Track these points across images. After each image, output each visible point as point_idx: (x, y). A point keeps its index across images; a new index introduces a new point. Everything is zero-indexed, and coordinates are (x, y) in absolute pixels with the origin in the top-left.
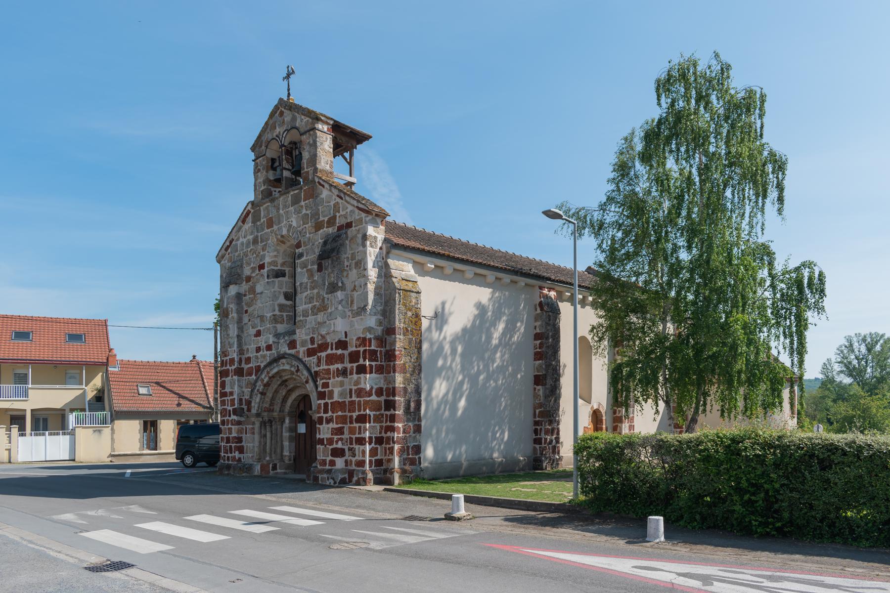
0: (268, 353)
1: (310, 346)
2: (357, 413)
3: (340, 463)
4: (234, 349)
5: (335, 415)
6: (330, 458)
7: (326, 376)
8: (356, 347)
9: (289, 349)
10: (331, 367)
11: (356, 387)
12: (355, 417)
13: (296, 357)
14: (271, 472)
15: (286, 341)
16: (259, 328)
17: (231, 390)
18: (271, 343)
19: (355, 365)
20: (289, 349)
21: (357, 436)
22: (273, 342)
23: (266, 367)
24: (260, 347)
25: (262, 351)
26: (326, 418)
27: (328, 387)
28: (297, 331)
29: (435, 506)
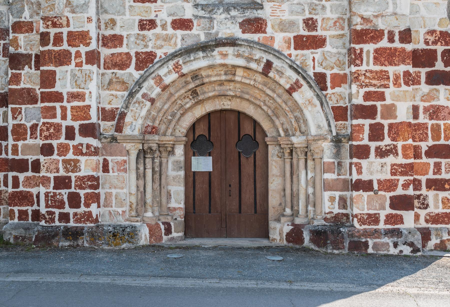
2: (431, 142)
8: (427, 43)
9: (243, 32)
10: (391, 70)
11: (427, 104)
14: (165, 238)
15: (234, 17)
20: (243, 32)
21: (431, 176)
28: (268, 6)
29: (370, 285)
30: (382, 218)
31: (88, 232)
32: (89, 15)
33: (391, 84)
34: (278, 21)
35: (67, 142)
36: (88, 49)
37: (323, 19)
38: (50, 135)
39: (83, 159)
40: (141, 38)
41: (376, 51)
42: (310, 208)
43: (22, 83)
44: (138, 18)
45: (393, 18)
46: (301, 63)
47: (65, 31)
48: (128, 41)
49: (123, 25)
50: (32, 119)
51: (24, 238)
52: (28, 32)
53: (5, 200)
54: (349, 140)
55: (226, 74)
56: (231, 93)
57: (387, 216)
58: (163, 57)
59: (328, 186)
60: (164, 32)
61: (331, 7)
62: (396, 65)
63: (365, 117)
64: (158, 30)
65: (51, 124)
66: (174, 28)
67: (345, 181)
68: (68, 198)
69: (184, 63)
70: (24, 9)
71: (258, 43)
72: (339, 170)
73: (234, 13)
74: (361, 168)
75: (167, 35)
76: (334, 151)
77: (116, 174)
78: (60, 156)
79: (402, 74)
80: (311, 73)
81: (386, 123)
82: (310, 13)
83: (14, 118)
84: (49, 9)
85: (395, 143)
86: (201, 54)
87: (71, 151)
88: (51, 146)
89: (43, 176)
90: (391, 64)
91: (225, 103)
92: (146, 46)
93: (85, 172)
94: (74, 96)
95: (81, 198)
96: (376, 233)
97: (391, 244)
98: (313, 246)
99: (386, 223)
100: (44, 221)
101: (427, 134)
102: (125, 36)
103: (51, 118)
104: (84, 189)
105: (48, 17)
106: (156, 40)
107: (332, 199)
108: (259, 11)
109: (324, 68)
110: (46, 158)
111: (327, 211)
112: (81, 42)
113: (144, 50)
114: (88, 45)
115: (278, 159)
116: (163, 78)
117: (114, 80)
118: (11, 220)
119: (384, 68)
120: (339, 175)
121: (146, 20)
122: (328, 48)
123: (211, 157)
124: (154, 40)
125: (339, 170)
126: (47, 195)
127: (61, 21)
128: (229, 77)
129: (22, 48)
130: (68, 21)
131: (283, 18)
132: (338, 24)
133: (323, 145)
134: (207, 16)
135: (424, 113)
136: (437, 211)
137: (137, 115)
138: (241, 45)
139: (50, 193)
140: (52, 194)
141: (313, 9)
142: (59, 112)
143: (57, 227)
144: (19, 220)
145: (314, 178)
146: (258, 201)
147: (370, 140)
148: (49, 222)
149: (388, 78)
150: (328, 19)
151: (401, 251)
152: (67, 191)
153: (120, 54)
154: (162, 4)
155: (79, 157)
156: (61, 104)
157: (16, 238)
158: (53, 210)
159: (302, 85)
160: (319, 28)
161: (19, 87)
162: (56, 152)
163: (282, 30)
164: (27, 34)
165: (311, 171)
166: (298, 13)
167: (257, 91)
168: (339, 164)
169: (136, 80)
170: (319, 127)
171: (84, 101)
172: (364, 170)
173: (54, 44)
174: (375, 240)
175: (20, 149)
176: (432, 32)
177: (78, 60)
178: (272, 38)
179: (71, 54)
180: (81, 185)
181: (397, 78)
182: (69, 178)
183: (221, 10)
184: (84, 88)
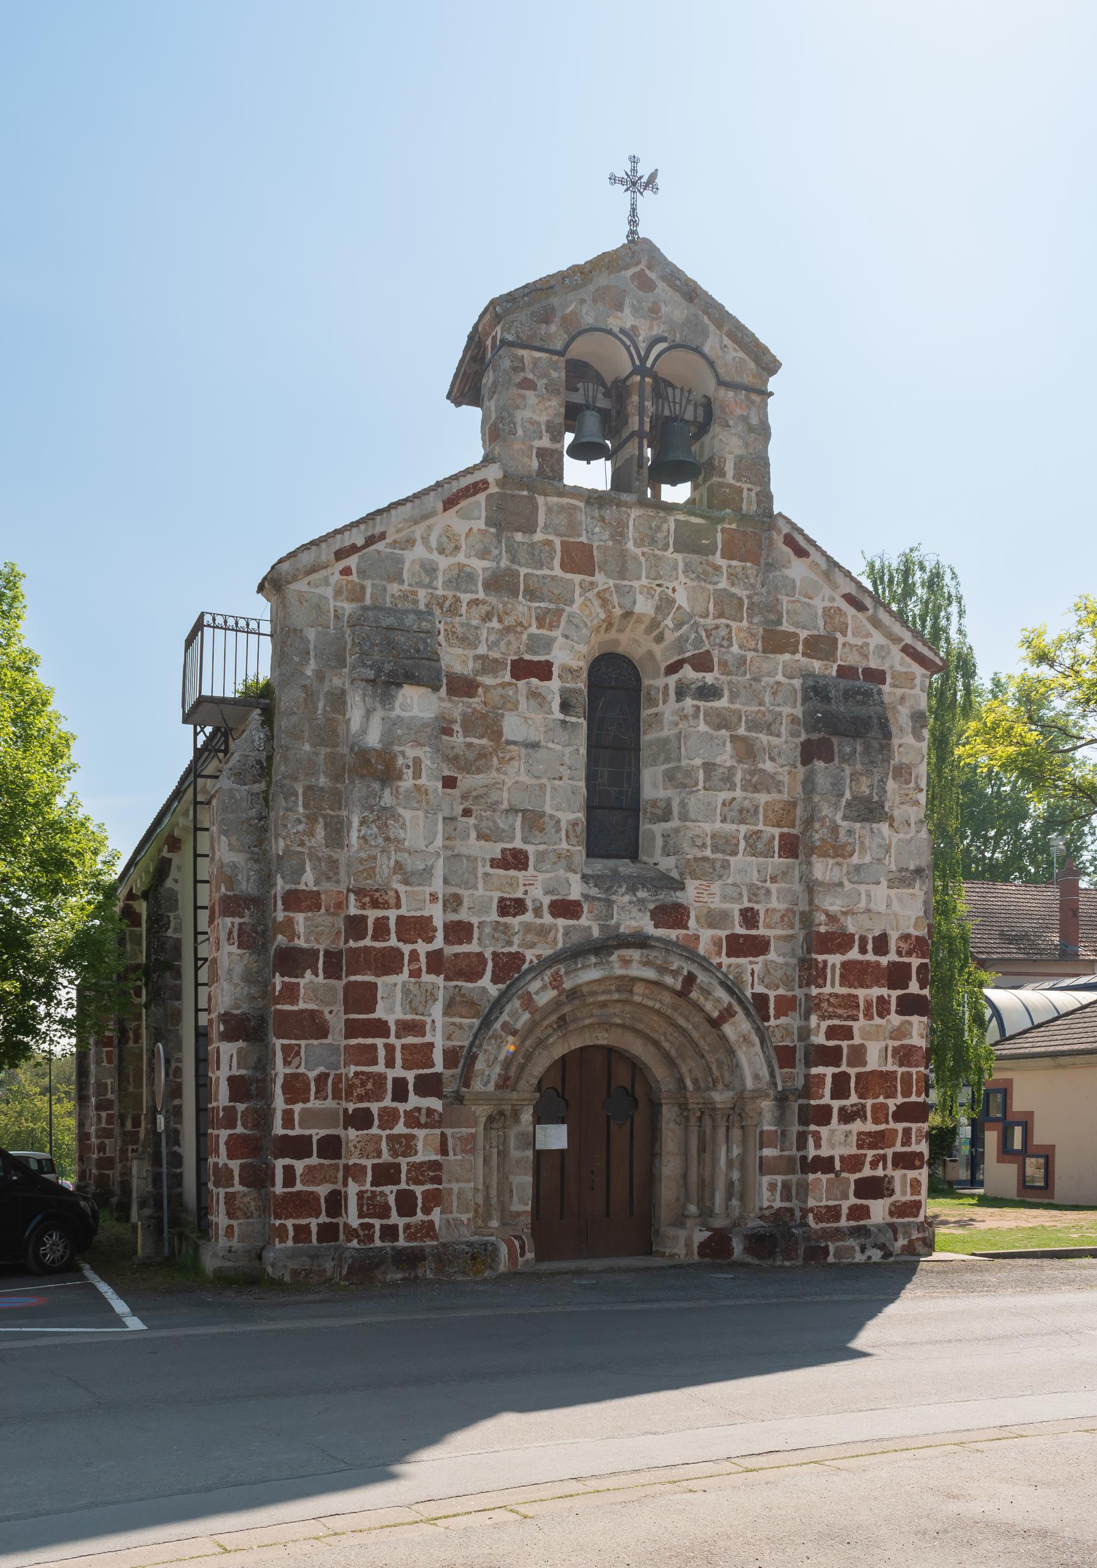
2: (900, 1100)
3: (879, 1210)
5: (869, 1103)
8: (899, 953)
9: (656, 926)
10: (862, 993)
11: (897, 1043)
12: (892, 1108)
13: (688, 951)
15: (642, 901)
16: (518, 844)
19: (895, 993)
20: (656, 926)
21: (899, 1148)
26: (842, 1110)
28: (692, 885)
30: (845, 1211)
31: (433, 1255)
32: (432, 890)
33: (861, 1015)
34: (705, 911)
35: (395, 1104)
36: (431, 947)
37: (767, 910)
38: (367, 1094)
39: (420, 1133)
40: (501, 928)
41: (844, 965)
42: (735, 1202)
43: (301, 1002)
44: (496, 895)
45: (865, 916)
46: (735, 978)
47: (392, 914)
48: (480, 933)
49: (472, 905)
50: (318, 1065)
51: (308, 1273)
52: (311, 910)
53: (241, 1210)
54: (800, 1097)
55: (618, 990)
56: (618, 1021)
57: (850, 1208)
58: (536, 961)
59: (764, 1167)
60: (538, 921)
61: (778, 892)
62: (868, 987)
63: (827, 1065)
64: (528, 917)
65: (369, 1075)
66: (554, 915)
67: (791, 1159)
68: (396, 1200)
69: (566, 973)
70: (303, 871)
71: (675, 944)
72: (783, 1142)
73: (642, 894)
74: (820, 1138)
75: (542, 925)
76: (777, 1114)
77: (459, 1157)
78: (384, 1129)
79: (875, 1000)
80: (748, 993)
81: (853, 1072)
82: (750, 900)
83: (287, 1063)
84: (365, 875)
85: (863, 1101)
86: (593, 959)
87: (402, 1120)
88: (368, 1111)
89: (355, 1164)
90: (862, 987)
91: (600, 1036)
92: (509, 943)
93: (424, 1154)
94: (407, 1028)
95: (417, 1198)
96: (838, 1234)
97: (858, 1248)
98: (749, 1259)
99: (849, 1218)
100: (355, 1241)
101: (895, 1087)
102: (476, 925)
103: (369, 1065)
104: (422, 1184)
105: (365, 889)
106: (525, 934)
107: (772, 1187)
108: (679, 894)
109: (766, 987)
110: (360, 1132)
111: (766, 1204)
112: (420, 936)
113: (506, 950)
114: (430, 940)
115: (677, 1126)
116: (534, 997)
117: (458, 999)
118: (280, 1242)
119: (853, 991)
120: (782, 1150)
121: (510, 899)
122: (772, 956)
123: (564, 1127)
124: (521, 933)
125: (783, 1142)
126: (360, 1195)
127: (386, 898)
128: (624, 996)
129: (302, 937)
130: (398, 897)
131: (712, 906)
132: (786, 919)
133: (762, 1105)
134: (603, 896)
135: (893, 1056)
136: (904, 1199)
137: (492, 1058)
138: (652, 947)
139: (366, 1192)
140: (369, 1194)
141: (754, 894)
142: (381, 1053)
143: (381, 1249)
144: (295, 1243)
145: (743, 1159)
147: (832, 1098)
148: (363, 1241)
149: (858, 1006)
150: (774, 910)
151: (869, 1258)
152: (395, 1188)
153: (468, 954)
154: (536, 873)
155: (415, 1131)
156: (385, 1040)
157: (295, 1273)
158: (371, 1221)
159: (736, 1012)
160: (761, 924)
161: (295, 1008)
162: (376, 1122)
163: (711, 926)
164: (310, 914)
165: (738, 1146)
166: (733, 900)
167: (655, 1018)
168: (783, 1133)
169: (492, 1000)
170: (756, 1077)
171: (423, 1035)
172: (824, 1142)
173: (375, 938)
174: (837, 1244)
175: (296, 1117)
176: (905, 937)
177: (414, 967)
178: (697, 938)
179: (402, 954)
180: (417, 1177)
181: (868, 1004)
182: (398, 1166)
183: (623, 890)
184: (423, 1014)
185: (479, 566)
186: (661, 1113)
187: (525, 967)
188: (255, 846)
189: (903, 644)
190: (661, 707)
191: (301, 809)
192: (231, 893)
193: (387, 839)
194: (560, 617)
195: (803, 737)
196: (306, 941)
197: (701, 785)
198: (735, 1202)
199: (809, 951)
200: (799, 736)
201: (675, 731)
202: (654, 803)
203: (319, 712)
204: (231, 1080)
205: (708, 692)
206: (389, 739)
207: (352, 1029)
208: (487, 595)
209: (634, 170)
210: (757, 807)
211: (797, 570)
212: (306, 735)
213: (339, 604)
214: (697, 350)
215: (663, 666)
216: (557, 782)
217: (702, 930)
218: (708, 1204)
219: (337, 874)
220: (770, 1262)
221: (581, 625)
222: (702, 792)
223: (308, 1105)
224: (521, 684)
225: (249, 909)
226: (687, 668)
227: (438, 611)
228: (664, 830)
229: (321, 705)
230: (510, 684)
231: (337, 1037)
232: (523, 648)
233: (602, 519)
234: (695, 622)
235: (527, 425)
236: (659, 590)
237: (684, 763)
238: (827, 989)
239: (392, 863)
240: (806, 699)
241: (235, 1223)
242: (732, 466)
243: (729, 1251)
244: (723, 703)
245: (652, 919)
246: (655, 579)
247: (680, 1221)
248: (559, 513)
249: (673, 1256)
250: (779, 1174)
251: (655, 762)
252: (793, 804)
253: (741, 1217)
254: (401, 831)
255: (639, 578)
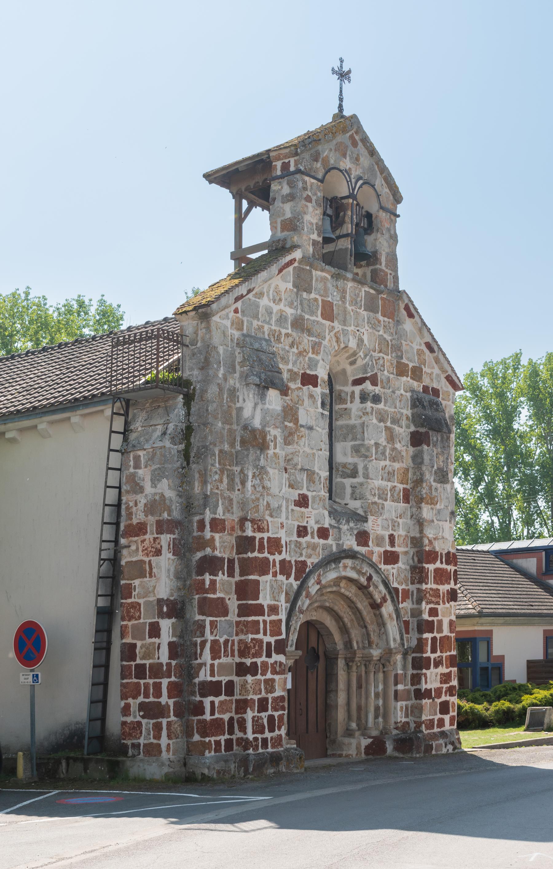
0: (322, 541)
1: (389, 548)
4: (280, 520)
5: (444, 655)
6: (439, 716)
7: (433, 599)
9: (358, 545)
13: (367, 559)
15: (351, 529)
16: (304, 491)
17: (273, 603)
18: (326, 526)
20: (358, 545)
22: (330, 525)
23: (317, 567)
24: (305, 528)
25: (309, 536)
27: (437, 615)
28: (371, 518)
34: (376, 535)
42: (380, 720)
44: (296, 523)
52: (221, 532)
53: (174, 733)
54: (413, 652)
72: (405, 681)
75: (314, 543)
76: (403, 663)
85: (442, 654)
90: (441, 584)
97: (444, 745)
98: (396, 754)
105: (254, 519)
112: (276, 551)
115: (343, 672)
120: (405, 686)
122: (400, 564)
131: (378, 532)
143: (263, 753)
146: (319, 721)
147: (431, 653)
149: (440, 596)
157: (218, 772)
174: (437, 742)
184: (278, 601)
185: (290, 311)
186: (337, 664)
187: (307, 570)
188: (180, 487)
189: (447, 374)
190: (349, 405)
191: (217, 465)
192: (169, 518)
193: (263, 487)
194: (321, 347)
195: (413, 429)
196: (220, 552)
197: (374, 457)
198: (380, 720)
199: (420, 561)
200: (409, 428)
201: (359, 421)
202: (345, 466)
203: (225, 401)
204: (170, 644)
205: (376, 399)
206: (265, 424)
207: (244, 611)
208: (292, 331)
209: (341, 67)
210: (394, 471)
211: (408, 325)
212: (220, 416)
213: (233, 332)
214: (373, 186)
215: (351, 379)
216: (320, 452)
217: (374, 548)
218: (363, 721)
219: (232, 508)
220: (410, 755)
221: (329, 353)
222: (374, 461)
223: (221, 661)
224: (305, 388)
225: (177, 529)
226: (368, 382)
227: (272, 340)
228: (352, 483)
229: (225, 397)
230: (300, 388)
231: (233, 616)
232: (306, 366)
233: (337, 287)
234: (371, 355)
235: (308, 224)
236: (358, 333)
237: (366, 442)
238: (429, 586)
239: (265, 503)
240: (414, 406)
241: (171, 742)
242: (385, 259)
243: (384, 750)
244: (381, 406)
245: (356, 541)
246: (356, 327)
247: (349, 733)
248: (321, 282)
249: (347, 756)
250: (403, 701)
251: (345, 439)
252: (407, 470)
253: (384, 728)
254: (268, 482)
255: (350, 326)
